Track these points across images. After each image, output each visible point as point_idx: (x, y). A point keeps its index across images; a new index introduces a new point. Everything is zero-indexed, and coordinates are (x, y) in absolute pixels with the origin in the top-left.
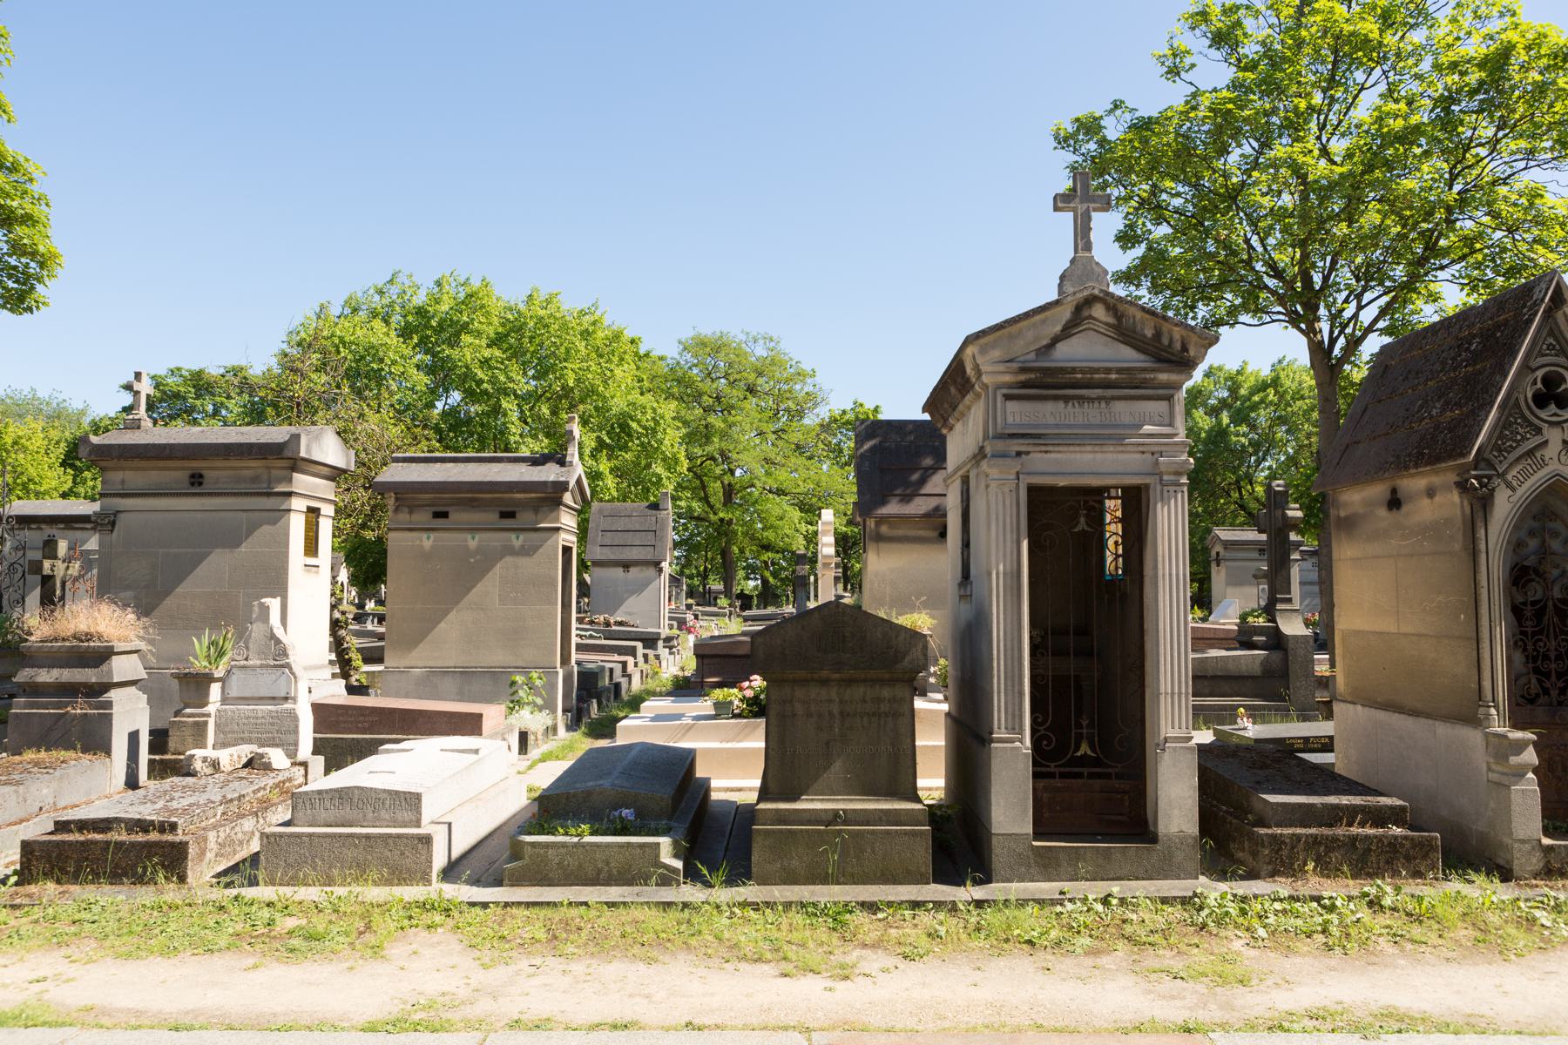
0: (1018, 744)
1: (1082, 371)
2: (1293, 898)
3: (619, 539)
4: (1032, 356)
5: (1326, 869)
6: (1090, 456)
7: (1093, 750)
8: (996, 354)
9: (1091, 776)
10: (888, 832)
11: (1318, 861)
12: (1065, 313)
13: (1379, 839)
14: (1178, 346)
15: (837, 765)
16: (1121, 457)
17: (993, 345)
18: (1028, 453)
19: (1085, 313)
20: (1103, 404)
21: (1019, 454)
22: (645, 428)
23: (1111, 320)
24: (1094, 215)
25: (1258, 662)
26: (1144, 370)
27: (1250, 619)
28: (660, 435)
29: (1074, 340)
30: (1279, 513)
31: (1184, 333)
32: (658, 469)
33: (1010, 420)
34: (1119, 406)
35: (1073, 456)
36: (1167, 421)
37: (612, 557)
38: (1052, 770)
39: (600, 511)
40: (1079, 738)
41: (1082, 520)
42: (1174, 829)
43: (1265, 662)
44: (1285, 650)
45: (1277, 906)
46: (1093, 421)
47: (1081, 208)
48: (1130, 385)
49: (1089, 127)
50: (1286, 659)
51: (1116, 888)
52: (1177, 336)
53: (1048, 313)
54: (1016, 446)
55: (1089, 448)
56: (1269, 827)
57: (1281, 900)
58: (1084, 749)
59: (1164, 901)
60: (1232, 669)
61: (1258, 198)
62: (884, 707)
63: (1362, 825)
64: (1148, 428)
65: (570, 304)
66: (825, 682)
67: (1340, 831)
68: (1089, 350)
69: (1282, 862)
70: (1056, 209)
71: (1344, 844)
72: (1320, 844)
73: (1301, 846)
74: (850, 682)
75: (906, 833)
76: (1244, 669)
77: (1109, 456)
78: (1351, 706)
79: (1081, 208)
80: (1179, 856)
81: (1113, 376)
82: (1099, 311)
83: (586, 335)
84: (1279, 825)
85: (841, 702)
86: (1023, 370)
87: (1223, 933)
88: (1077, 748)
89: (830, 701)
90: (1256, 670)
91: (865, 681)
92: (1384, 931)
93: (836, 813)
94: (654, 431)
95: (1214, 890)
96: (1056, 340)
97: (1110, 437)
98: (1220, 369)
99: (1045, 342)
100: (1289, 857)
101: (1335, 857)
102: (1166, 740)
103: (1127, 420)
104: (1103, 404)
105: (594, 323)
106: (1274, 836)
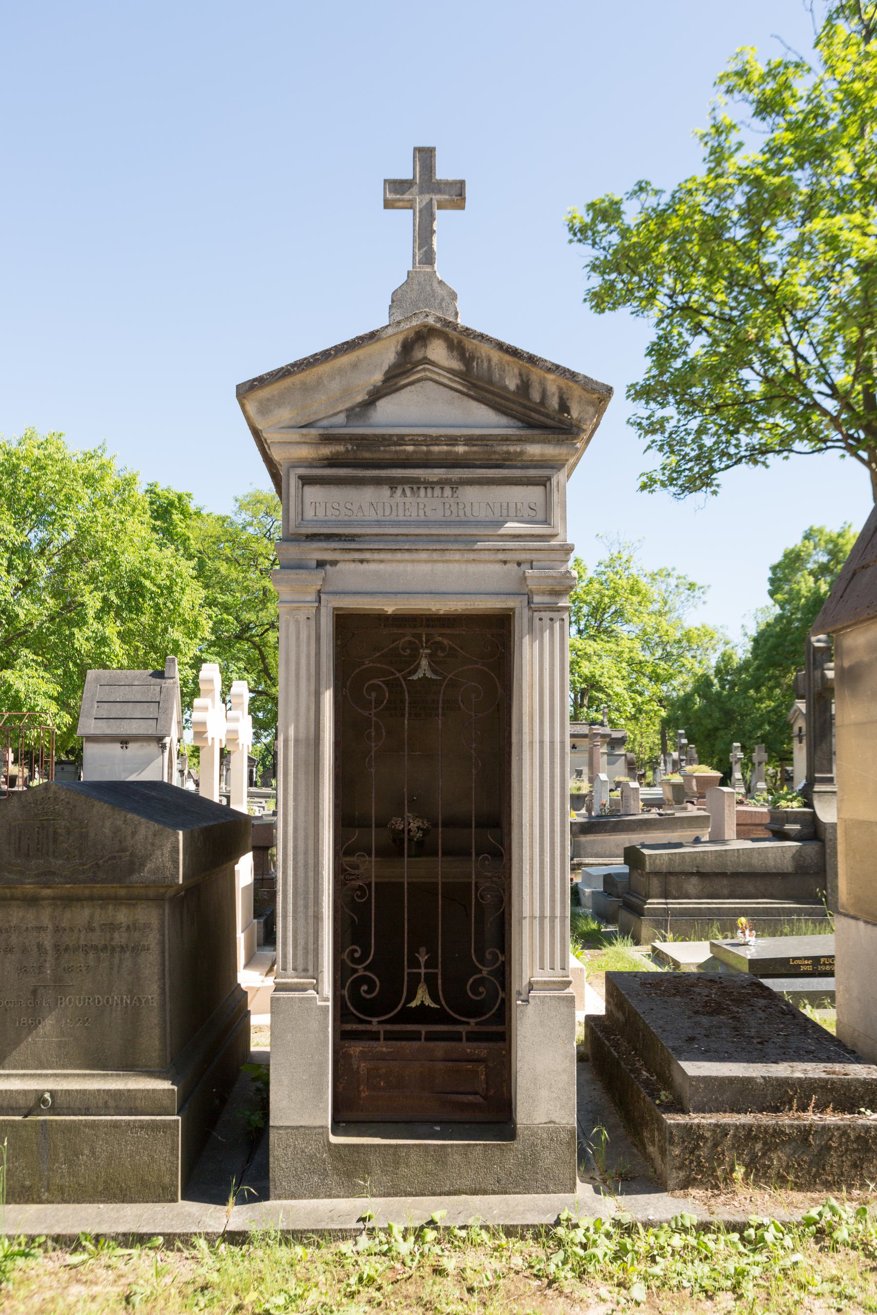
0: (311, 993)
1: (415, 441)
2: (704, 1227)
3: (117, 711)
4: (341, 419)
5: (760, 1173)
6: (428, 567)
7: (434, 997)
8: (285, 414)
9: (431, 1037)
10: (115, 1125)
11: (751, 1166)
12: (387, 354)
13: (843, 1131)
14: (554, 403)
15: (49, 1024)
16: (472, 568)
17: (279, 401)
18: (334, 563)
19: (418, 354)
20: (448, 491)
21: (321, 564)
22: (159, 586)
23: (456, 365)
24: (439, 214)
25: (789, 856)
26: (506, 439)
27: (783, 803)
28: (177, 595)
29: (404, 396)
30: (818, 674)
31: (562, 382)
32: (176, 634)
33: (309, 514)
34: (470, 494)
35: (401, 567)
36: (540, 516)
37: (108, 731)
38: (374, 1027)
39: (97, 679)
40: (414, 981)
41: (424, 663)
42: (539, 1118)
43: (798, 856)
44: (822, 841)
45: (677, 1241)
46: (432, 516)
47: (420, 201)
48: (484, 462)
49: (607, 213)
50: (823, 853)
51: (440, 1209)
52: (552, 389)
53: (360, 353)
54: (315, 552)
55: (424, 556)
56: (683, 1111)
57: (685, 1230)
58: (422, 997)
59: (510, 1231)
60: (757, 864)
61: (798, 289)
62: (120, 938)
63: (821, 1108)
64: (512, 527)
65: (74, 448)
66: (32, 901)
67: (786, 1119)
68: (426, 409)
69: (701, 1167)
70: (388, 204)
71: (791, 1139)
72: (756, 1138)
73: (728, 1141)
74: (69, 901)
75: (142, 1126)
76: (771, 864)
77: (455, 567)
78: (852, 922)
79: (420, 201)
80: (547, 1159)
81: (461, 449)
82: (437, 351)
83: (89, 480)
84: (701, 1109)
85: (57, 929)
86: (327, 439)
87: (584, 1292)
88: (412, 996)
89: (40, 929)
90: (788, 865)
91: (91, 898)
92: (827, 1287)
93: (39, 1096)
94: (170, 589)
95: (592, 1208)
96: (375, 396)
97: (456, 539)
98: (821, 531)
99: (360, 398)
100: (710, 1159)
101: (777, 1159)
102: (531, 987)
103: (482, 514)
104: (448, 491)
105: (102, 467)
106: (688, 1129)
